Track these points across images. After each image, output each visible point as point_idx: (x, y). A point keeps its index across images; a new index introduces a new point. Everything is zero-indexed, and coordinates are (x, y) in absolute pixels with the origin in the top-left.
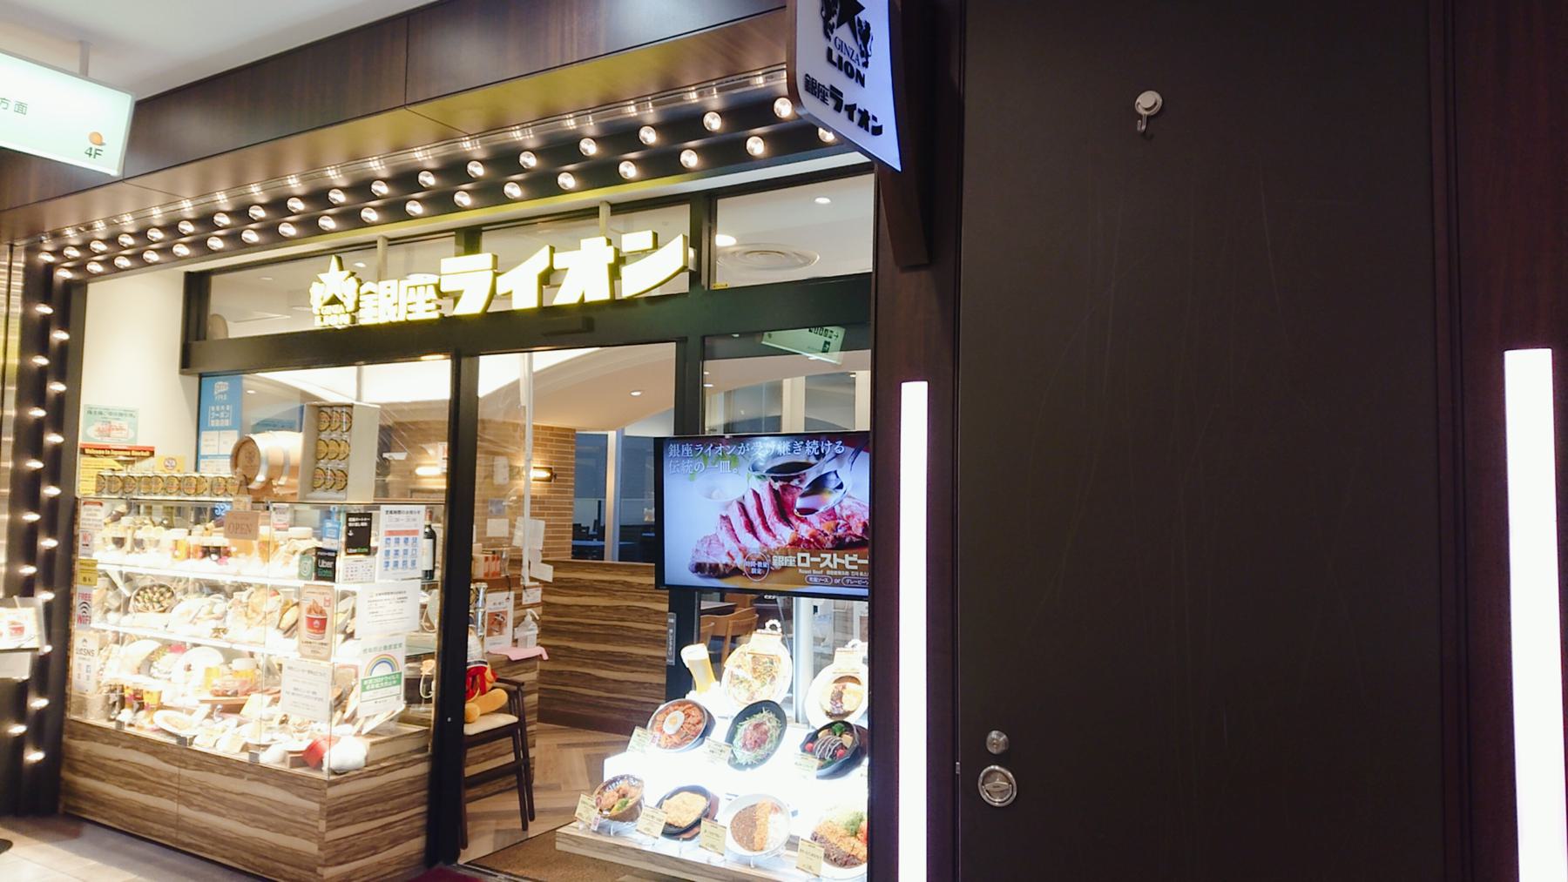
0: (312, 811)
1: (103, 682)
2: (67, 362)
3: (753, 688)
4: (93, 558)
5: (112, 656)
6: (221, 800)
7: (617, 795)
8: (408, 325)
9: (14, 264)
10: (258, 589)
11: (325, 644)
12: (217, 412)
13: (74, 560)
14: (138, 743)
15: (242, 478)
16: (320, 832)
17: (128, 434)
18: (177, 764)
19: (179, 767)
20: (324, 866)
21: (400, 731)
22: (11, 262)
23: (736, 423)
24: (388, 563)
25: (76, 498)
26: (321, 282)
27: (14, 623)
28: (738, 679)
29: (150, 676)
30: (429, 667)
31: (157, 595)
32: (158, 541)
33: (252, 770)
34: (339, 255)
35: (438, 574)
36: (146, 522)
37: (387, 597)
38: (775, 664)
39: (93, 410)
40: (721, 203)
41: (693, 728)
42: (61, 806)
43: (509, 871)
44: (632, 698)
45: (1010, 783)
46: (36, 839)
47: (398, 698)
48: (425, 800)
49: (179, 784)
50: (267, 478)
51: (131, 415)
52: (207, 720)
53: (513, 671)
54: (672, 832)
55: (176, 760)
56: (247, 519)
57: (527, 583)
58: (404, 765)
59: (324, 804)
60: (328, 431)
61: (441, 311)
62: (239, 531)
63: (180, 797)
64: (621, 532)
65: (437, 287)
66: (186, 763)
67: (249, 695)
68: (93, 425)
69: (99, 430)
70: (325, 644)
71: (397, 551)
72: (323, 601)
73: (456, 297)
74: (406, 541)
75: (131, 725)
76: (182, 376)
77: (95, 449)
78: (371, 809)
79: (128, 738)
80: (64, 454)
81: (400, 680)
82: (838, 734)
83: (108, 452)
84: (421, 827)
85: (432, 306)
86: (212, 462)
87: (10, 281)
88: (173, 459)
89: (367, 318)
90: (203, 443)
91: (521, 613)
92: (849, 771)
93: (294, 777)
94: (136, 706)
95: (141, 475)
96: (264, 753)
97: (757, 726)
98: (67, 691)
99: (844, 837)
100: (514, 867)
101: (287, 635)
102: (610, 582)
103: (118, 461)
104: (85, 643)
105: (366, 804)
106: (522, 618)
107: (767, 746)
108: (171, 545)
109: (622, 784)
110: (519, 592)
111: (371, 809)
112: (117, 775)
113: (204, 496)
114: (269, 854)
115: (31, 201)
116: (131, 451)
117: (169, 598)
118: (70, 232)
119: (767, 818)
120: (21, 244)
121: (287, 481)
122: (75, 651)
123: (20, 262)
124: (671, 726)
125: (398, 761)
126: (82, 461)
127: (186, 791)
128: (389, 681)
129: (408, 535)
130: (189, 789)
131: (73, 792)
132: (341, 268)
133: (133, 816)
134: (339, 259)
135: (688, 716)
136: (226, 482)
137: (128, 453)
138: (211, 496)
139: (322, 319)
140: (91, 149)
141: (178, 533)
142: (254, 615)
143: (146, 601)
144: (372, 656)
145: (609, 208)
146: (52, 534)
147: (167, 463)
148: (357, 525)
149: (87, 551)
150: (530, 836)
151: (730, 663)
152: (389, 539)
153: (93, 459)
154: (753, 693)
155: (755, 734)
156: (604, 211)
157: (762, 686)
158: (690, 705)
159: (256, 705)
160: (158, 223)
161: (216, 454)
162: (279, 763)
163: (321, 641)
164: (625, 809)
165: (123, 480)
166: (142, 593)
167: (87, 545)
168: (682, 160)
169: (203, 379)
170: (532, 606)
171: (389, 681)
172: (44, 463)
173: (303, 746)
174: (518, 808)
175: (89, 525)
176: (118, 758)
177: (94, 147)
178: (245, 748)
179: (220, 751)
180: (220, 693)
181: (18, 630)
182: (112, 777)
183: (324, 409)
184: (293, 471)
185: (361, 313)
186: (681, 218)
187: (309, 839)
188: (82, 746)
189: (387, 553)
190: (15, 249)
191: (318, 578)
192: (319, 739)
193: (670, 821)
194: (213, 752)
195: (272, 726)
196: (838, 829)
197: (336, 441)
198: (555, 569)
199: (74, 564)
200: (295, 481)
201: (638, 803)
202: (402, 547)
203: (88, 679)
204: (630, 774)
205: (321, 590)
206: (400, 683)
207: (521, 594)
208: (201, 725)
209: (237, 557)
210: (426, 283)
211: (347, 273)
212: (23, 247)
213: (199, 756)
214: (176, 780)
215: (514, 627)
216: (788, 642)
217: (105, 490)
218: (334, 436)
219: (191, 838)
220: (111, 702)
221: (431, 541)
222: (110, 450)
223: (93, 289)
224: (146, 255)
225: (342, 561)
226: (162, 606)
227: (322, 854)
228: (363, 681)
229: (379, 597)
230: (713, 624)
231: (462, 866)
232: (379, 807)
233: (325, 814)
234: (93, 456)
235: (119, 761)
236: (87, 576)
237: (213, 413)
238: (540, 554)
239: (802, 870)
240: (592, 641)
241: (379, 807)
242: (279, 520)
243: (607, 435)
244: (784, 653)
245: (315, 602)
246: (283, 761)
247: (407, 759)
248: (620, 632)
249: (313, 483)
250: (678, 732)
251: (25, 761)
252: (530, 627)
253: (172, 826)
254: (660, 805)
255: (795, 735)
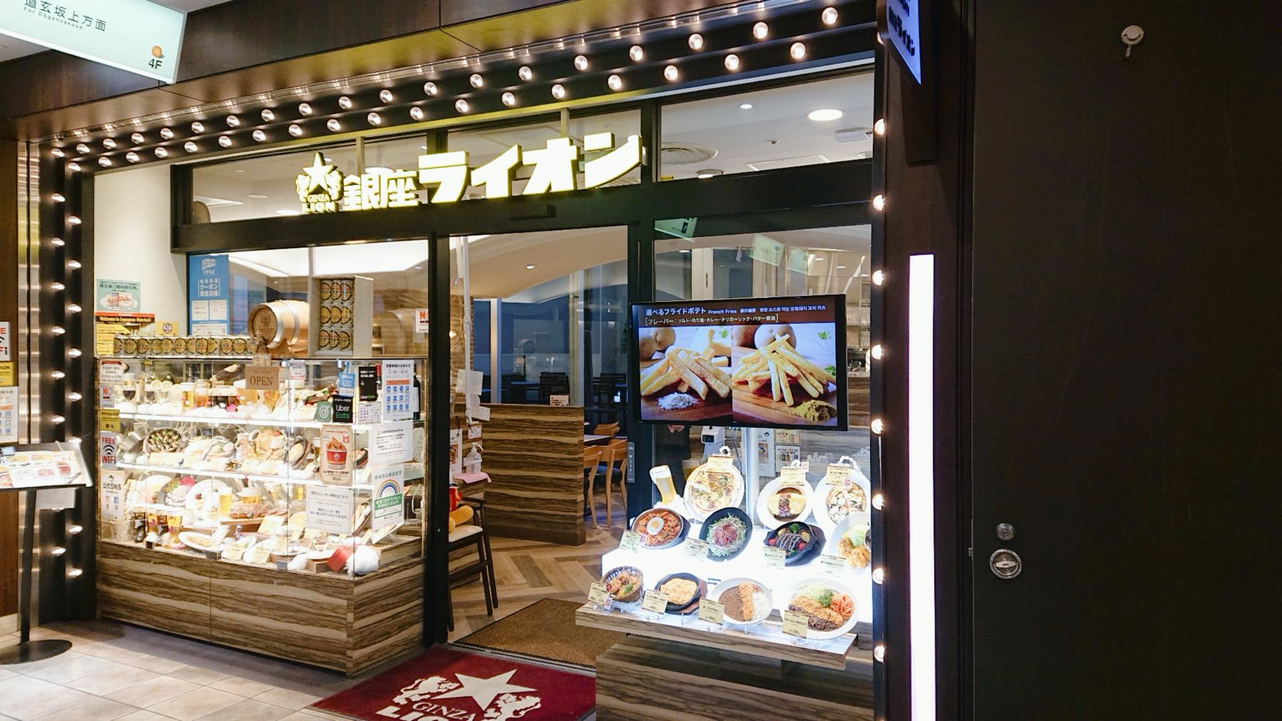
0: (339, 607)
1: (128, 511)
2: (81, 243)
3: (713, 499)
4: (115, 408)
5: (130, 489)
6: (253, 603)
7: (620, 582)
8: (389, 211)
9: (31, 160)
10: (262, 432)
11: (346, 473)
12: (206, 285)
13: (97, 410)
14: (167, 559)
15: (261, 340)
16: (349, 623)
17: (133, 304)
18: (209, 575)
19: (210, 577)
20: (354, 649)
21: (398, 541)
22: (28, 158)
23: (594, 289)
24: (389, 406)
25: (96, 359)
26: (306, 175)
27: (60, 464)
28: (698, 492)
29: (166, 504)
30: (421, 491)
31: (166, 438)
32: (167, 393)
33: (281, 576)
34: (321, 151)
35: (423, 415)
36: (152, 377)
37: (390, 434)
38: (729, 480)
39: (104, 284)
40: (664, 108)
41: (672, 530)
42: (98, 613)
43: (492, 646)
44: (542, 511)
45: (1017, 561)
46: (87, 638)
47: (400, 515)
48: (422, 594)
49: (210, 590)
50: (281, 339)
51: (135, 288)
52: (228, 539)
53: (467, 491)
54: (673, 608)
55: (206, 571)
56: (267, 373)
57: (472, 423)
58: (406, 567)
59: (352, 600)
60: (330, 300)
61: (419, 200)
62: (260, 383)
63: (211, 601)
64: (502, 380)
65: (416, 180)
66: (217, 574)
67: (264, 517)
68: (105, 296)
69: (109, 301)
70: (346, 473)
71: (395, 397)
72: (342, 439)
73: (432, 191)
74: (401, 389)
75: (158, 545)
76: (174, 254)
77: (108, 317)
78: (384, 602)
79: (157, 555)
80: (83, 320)
81: (400, 501)
82: (795, 532)
83: (118, 320)
84: (419, 615)
85: (412, 195)
86: (204, 326)
87: (28, 174)
88: (169, 325)
89: (350, 205)
90: (193, 310)
91: (468, 445)
92: (811, 560)
93: (322, 580)
94: (160, 529)
95: (152, 338)
96: (291, 562)
97: (726, 527)
98: (97, 518)
99: (819, 608)
100: (494, 643)
101: (296, 466)
102: (519, 421)
103: (126, 327)
104: (111, 479)
105: (382, 598)
106: (469, 450)
107: (738, 542)
108: (182, 396)
109: (625, 574)
110: (465, 429)
111: (384, 602)
112: (151, 586)
113: (215, 355)
114: (301, 643)
115: (64, 104)
116: (136, 318)
117: (177, 440)
118: (109, 128)
119: (751, 596)
120: (36, 141)
121: (297, 342)
122: (102, 486)
123: (36, 157)
124: (654, 529)
125: (401, 564)
126: (98, 327)
127: (218, 596)
128: (393, 501)
129: (403, 384)
130: (220, 595)
131: (110, 600)
132: (324, 163)
133: (168, 618)
134: (322, 156)
135: (666, 521)
136: (233, 343)
137: (134, 320)
138: (220, 355)
139: (309, 207)
140: (153, 60)
141: (186, 386)
142: (262, 452)
143: (158, 443)
144: (381, 482)
145: (568, 114)
146: (76, 389)
147: (165, 328)
148: (366, 376)
149: (109, 403)
150: (496, 620)
151: (691, 481)
152: (389, 387)
153: (107, 325)
154: (713, 503)
155: (727, 533)
156: (564, 116)
157: (720, 497)
158: (665, 513)
159: (271, 524)
160: (169, 124)
161: (207, 319)
162: (304, 569)
163: (342, 470)
164: (631, 592)
165: (137, 342)
166: (153, 436)
167: (108, 398)
168: (665, 74)
169: (191, 257)
170: (475, 440)
171: (393, 501)
172: (65, 329)
173: (328, 554)
174: (484, 598)
175: (109, 380)
176: (150, 572)
177: (156, 59)
178: (271, 559)
179: (248, 561)
180: (238, 516)
181: (65, 469)
182: (145, 587)
183: (326, 282)
184: (303, 333)
185: (346, 201)
186: (634, 118)
187: (338, 629)
188: (112, 562)
189: (389, 399)
190: (31, 145)
191: (335, 420)
192: (342, 549)
193: (670, 601)
194: (240, 563)
195: (293, 540)
196: (813, 602)
197: (338, 308)
198: (491, 412)
199: (97, 414)
200: (303, 341)
201: (641, 588)
202: (398, 394)
203: (117, 508)
204: (628, 565)
205: (340, 430)
206: (400, 502)
207: (467, 432)
208: (223, 543)
209: (246, 404)
210: (395, 177)
211: (330, 167)
212: (37, 144)
213: (228, 567)
214: (207, 588)
215: (463, 457)
216: (738, 464)
217: (122, 351)
218: (336, 304)
219: (224, 633)
220: (136, 526)
221: (417, 388)
222: (119, 317)
223: (100, 181)
224: (157, 152)
225: (358, 406)
226: (172, 447)
227: (351, 640)
228: (376, 501)
229: (384, 435)
230: (600, 453)
231: (452, 645)
232: (390, 601)
233: (353, 607)
234: (106, 322)
235: (152, 574)
236: (110, 423)
237: (202, 286)
238: (479, 399)
239: (789, 634)
240: (506, 467)
241: (390, 601)
242: (297, 374)
243: (490, 302)
244: (735, 473)
245: (334, 439)
246: (307, 568)
247: (408, 562)
248: (530, 460)
249: (319, 342)
250: (660, 533)
251: (67, 578)
252: (477, 456)
253: (206, 625)
254: (658, 588)
255: (759, 535)
